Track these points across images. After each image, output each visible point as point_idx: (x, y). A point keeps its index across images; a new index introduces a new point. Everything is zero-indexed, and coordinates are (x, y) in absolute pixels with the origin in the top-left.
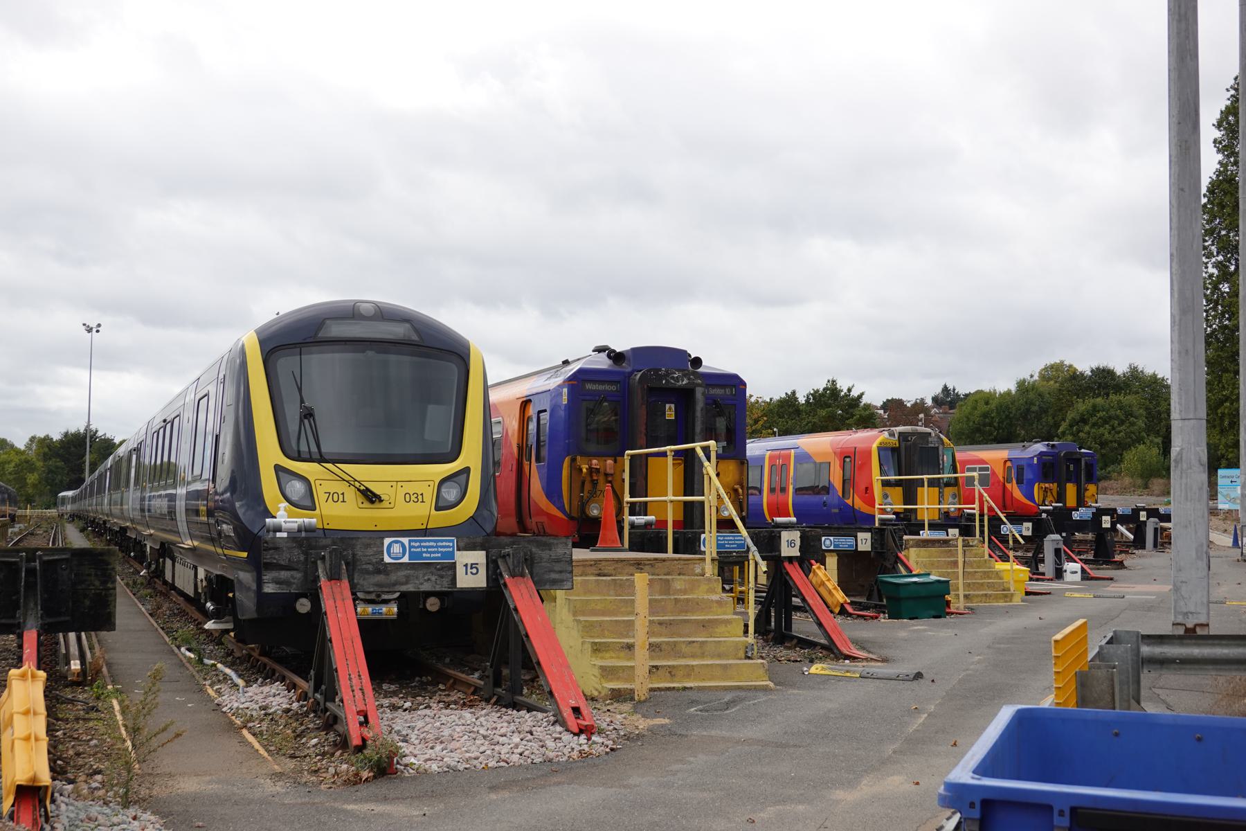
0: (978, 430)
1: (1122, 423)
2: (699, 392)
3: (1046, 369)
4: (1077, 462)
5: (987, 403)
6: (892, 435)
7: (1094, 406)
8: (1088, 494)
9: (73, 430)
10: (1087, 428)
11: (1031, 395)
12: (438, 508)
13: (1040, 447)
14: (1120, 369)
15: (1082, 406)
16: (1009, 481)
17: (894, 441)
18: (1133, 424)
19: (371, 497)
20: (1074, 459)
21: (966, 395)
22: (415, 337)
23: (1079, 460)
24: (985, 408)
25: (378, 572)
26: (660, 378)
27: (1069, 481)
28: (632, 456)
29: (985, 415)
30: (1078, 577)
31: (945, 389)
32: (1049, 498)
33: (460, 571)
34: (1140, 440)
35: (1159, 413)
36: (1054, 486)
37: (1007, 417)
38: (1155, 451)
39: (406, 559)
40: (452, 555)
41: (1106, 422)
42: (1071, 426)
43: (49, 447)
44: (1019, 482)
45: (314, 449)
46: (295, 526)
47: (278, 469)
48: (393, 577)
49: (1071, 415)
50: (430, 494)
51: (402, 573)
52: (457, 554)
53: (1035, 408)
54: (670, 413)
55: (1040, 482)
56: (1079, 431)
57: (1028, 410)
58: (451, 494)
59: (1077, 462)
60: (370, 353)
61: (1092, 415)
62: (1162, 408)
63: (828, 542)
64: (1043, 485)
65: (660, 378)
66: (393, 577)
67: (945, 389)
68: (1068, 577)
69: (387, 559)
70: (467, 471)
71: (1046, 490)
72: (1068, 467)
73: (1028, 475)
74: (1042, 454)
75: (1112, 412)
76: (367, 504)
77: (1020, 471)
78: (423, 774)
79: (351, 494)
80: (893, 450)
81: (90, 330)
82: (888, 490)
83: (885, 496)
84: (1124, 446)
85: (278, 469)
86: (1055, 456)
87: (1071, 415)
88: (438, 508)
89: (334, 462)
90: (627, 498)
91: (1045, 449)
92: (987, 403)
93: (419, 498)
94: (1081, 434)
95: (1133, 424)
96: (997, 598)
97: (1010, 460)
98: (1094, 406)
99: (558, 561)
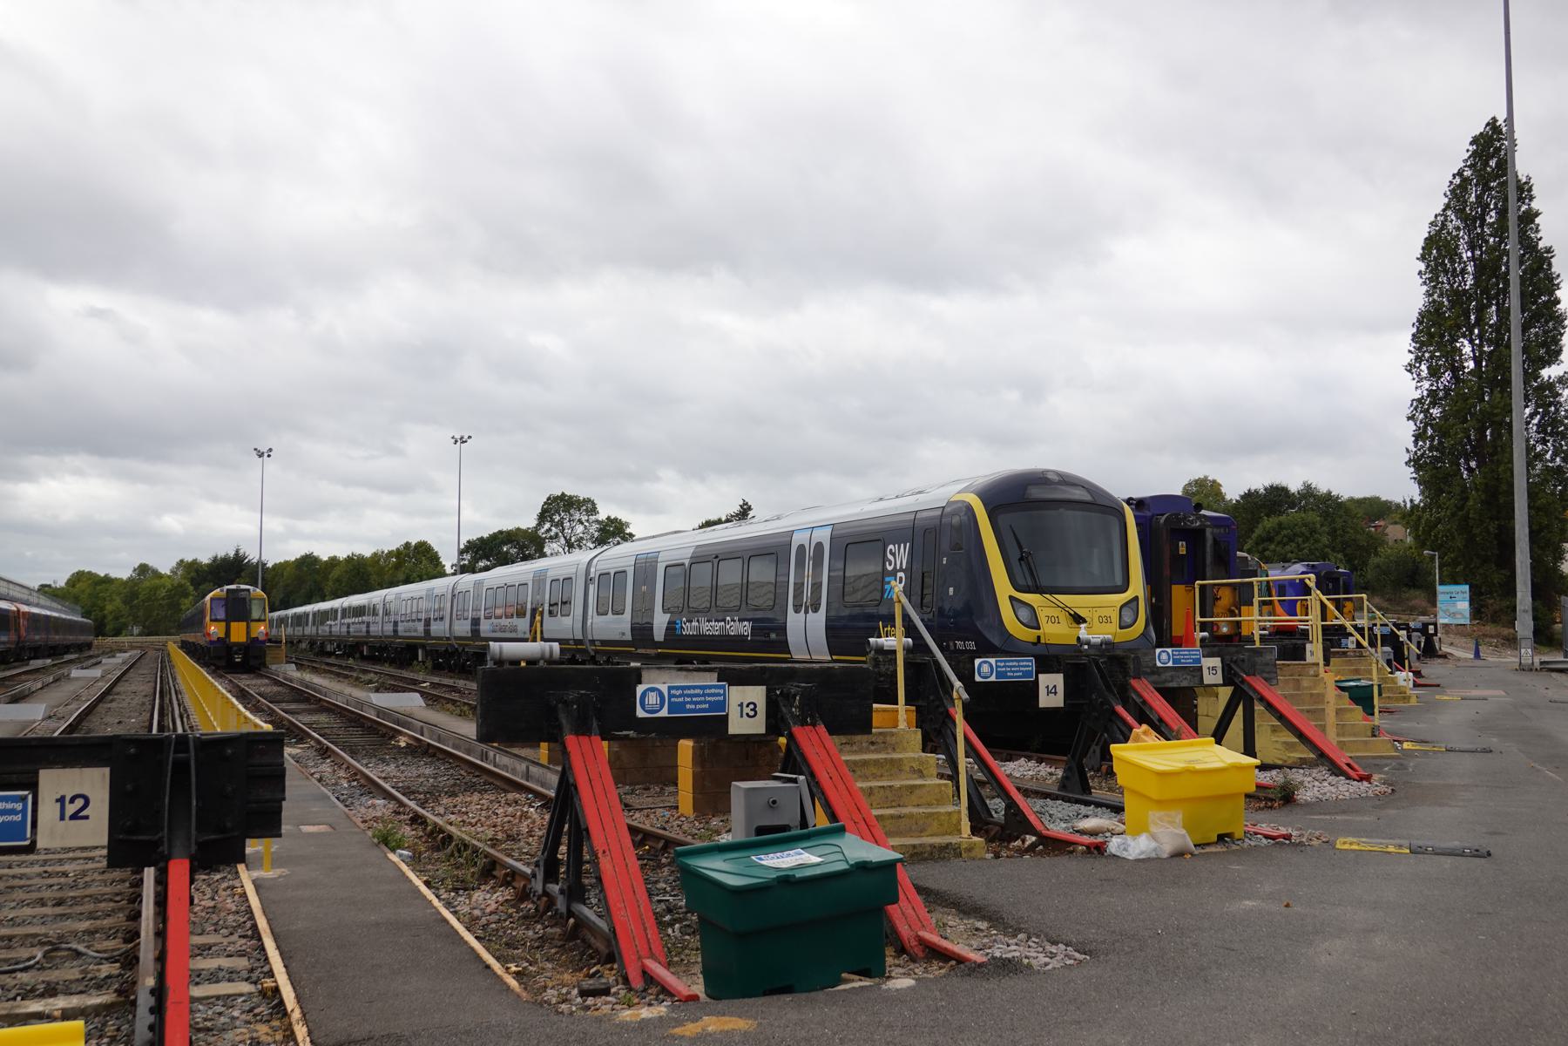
1: (1306, 540)
2: (1208, 531)
7: (1280, 524)
9: (221, 554)
10: (1272, 547)
14: (1294, 486)
15: (1269, 523)
18: (1317, 541)
19: (1078, 619)
23: (1337, 580)
25: (1153, 673)
26: (1179, 520)
28: (1202, 587)
33: (1205, 672)
39: (1170, 664)
40: (1199, 661)
41: (1291, 540)
42: (1257, 544)
43: (197, 571)
47: (1011, 598)
48: (1163, 677)
49: (1258, 532)
50: (1115, 619)
51: (1169, 674)
54: (1182, 549)
56: (1265, 550)
61: (1278, 533)
63: (985, 668)
65: (1179, 520)
66: (1163, 677)
70: (1136, 598)
75: (1297, 530)
79: (1063, 616)
81: (261, 455)
85: (1011, 598)
90: (1198, 618)
93: (1108, 620)
95: (1317, 541)
96: (1397, 700)
98: (1280, 524)
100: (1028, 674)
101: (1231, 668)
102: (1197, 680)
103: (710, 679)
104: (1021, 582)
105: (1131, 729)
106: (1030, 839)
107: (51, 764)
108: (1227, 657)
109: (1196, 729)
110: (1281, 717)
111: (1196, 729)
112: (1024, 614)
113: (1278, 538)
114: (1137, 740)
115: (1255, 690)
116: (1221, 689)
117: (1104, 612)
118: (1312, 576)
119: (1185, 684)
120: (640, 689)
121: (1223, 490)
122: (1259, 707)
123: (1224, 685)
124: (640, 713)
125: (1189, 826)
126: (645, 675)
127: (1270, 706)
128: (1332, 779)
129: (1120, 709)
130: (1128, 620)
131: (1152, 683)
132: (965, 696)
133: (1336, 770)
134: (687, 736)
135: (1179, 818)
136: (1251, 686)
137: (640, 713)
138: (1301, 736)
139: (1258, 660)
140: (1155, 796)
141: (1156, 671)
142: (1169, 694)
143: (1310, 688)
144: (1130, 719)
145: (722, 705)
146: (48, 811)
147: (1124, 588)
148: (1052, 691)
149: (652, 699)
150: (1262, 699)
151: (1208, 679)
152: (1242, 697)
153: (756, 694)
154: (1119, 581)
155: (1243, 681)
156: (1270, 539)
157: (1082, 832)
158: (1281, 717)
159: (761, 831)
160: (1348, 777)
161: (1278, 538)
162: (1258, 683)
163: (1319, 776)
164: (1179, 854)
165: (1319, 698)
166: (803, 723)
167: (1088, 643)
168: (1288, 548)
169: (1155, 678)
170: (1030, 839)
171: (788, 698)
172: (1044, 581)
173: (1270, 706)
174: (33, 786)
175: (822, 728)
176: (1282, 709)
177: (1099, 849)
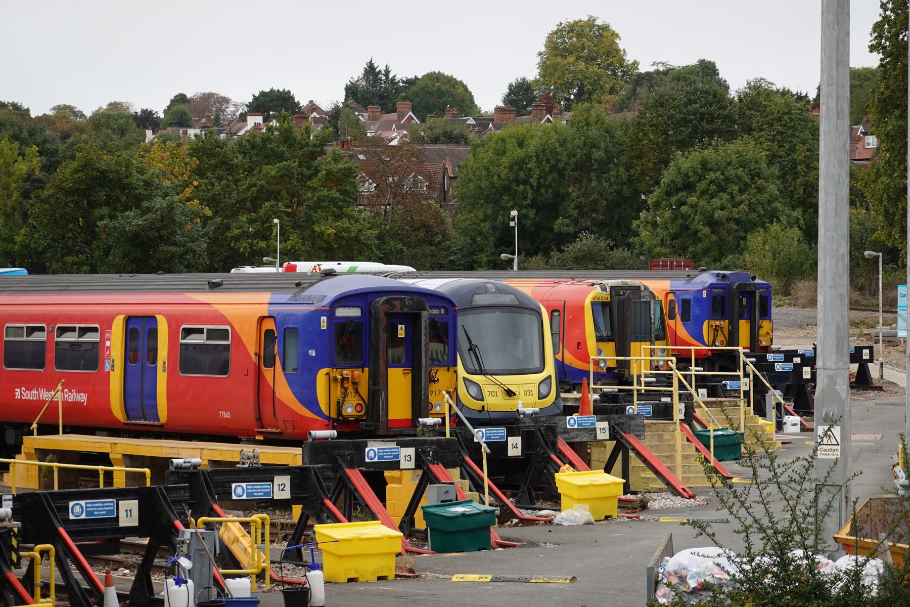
0: (506, 189)
3: (559, 32)
4: (751, 295)
5: (521, 144)
6: (604, 289)
7: (704, 164)
8: (762, 332)
10: (692, 199)
11: (594, 132)
12: (539, 398)
13: (707, 278)
15: (685, 161)
16: (672, 316)
17: (606, 296)
18: (760, 190)
19: (510, 393)
20: (747, 292)
21: (410, 83)
22: (517, 303)
23: (754, 292)
24: (519, 153)
25: (565, 433)
27: (741, 317)
29: (520, 164)
30: (797, 429)
31: (371, 70)
32: (720, 338)
33: (598, 431)
34: (773, 216)
35: (794, 163)
36: (725, 324)
37: (554, 168)
38: (796, 233)
39: (576, 427)
42: (669, 194)
44: (685, 318)
45: (477, 367)
46: (530, 412)
48: (571, 435)
49: (668, 176)
52: (597, 423)
53: (598, 154)
55: (710, 319)
57: (588, 157)
58: (544, 390)
59: (751, 295)
60: (498, 313)
61: (701, 177)
62: (800, 154)
64: (713, 323)
66: (571, 435)
67: (371, 70)
68: (788, 429)
69: (568, 427)
70: (550, 377)
71: (716, 329)
72: (741, 300)
73: (695, 311)
74: (712, 286)
75: (731, 172)
76: (507, 397)
77: (686, 303)
78: (655, 510)
79: (500, 392)
80: (604, 305)
82: (603, 345)
83: (600, 352)
84: (747, 226)
85: (465, 379)
86: (727, 288)
87: (668, 176)
88: (539, 398)
89: (491, 375)
91: (713, 280)
92: (521, 144)
93: (530, 393)
94: (684, 209)
95: (760, 190)
97: (673, 292)
98: (704, 164)
99: (638, 426)
100: (501, 437)
101: (614, 429)
102: (592, 437)
103: (393, 445)
104: (471, 367)
105: (559, 467)
106: (515, 521)
107: (122, 489)
108: (612, 422)
109: (589, 465)
110: (645, 461)
111: (589, 465)
112: (473, 391)
113: (701, 186)
114: (563, 471)
115: (629, 443)
116: (608, 442)
117: (527, 388)
118: (674, 359)
119: (585, 439)
120: (367, 450)
121: (621, 44)
122: (631, 454)
123: (610, 439)
124: (367, 460)
125: (592, 511)
126: (369, 443)
127: (638, 454)
128: (674, 498)
129: (553, 456)
130: (544, 392)
131: (564, 439)
132: (488, 451)
133: (676, 492)
134: (515, 459)
135: (587, 508)
136: (627, 440)
137: (367, 460)
138: (656, 472)
139: (632, 423)
140: (576, 497)
141: (566, 431)
142: (573, 445)
143: (669, 440)
144: (62, 603)
145: (398, 456)
146: (276, 488)
147: (541, 370)
148: (515, 447)
149: (372, 454)
150: (634, 449)
151: (600, 436)
152: (621, 448)
153: (411, 451)
154: (537, 364)
155: (622, 437)
156: (688, 187)
157: (541, 516)
158: (645, 461)
159: (442, 501)
160: (683, 497)
161: (701, 186)
162: (631, 438)
163: (666, 497)
164: (588, 523)
165: (672, 447)
166: (434, 463)
167: (524, 414)
168: (716, 202)
169: (566, 436)
170: (515, 521)
171: (426, 453)
172: (487, 367)
173: (638, 454)
174: (272, 481)
175: (441, 465)
176: (645, 455)
177: (550, 522)
